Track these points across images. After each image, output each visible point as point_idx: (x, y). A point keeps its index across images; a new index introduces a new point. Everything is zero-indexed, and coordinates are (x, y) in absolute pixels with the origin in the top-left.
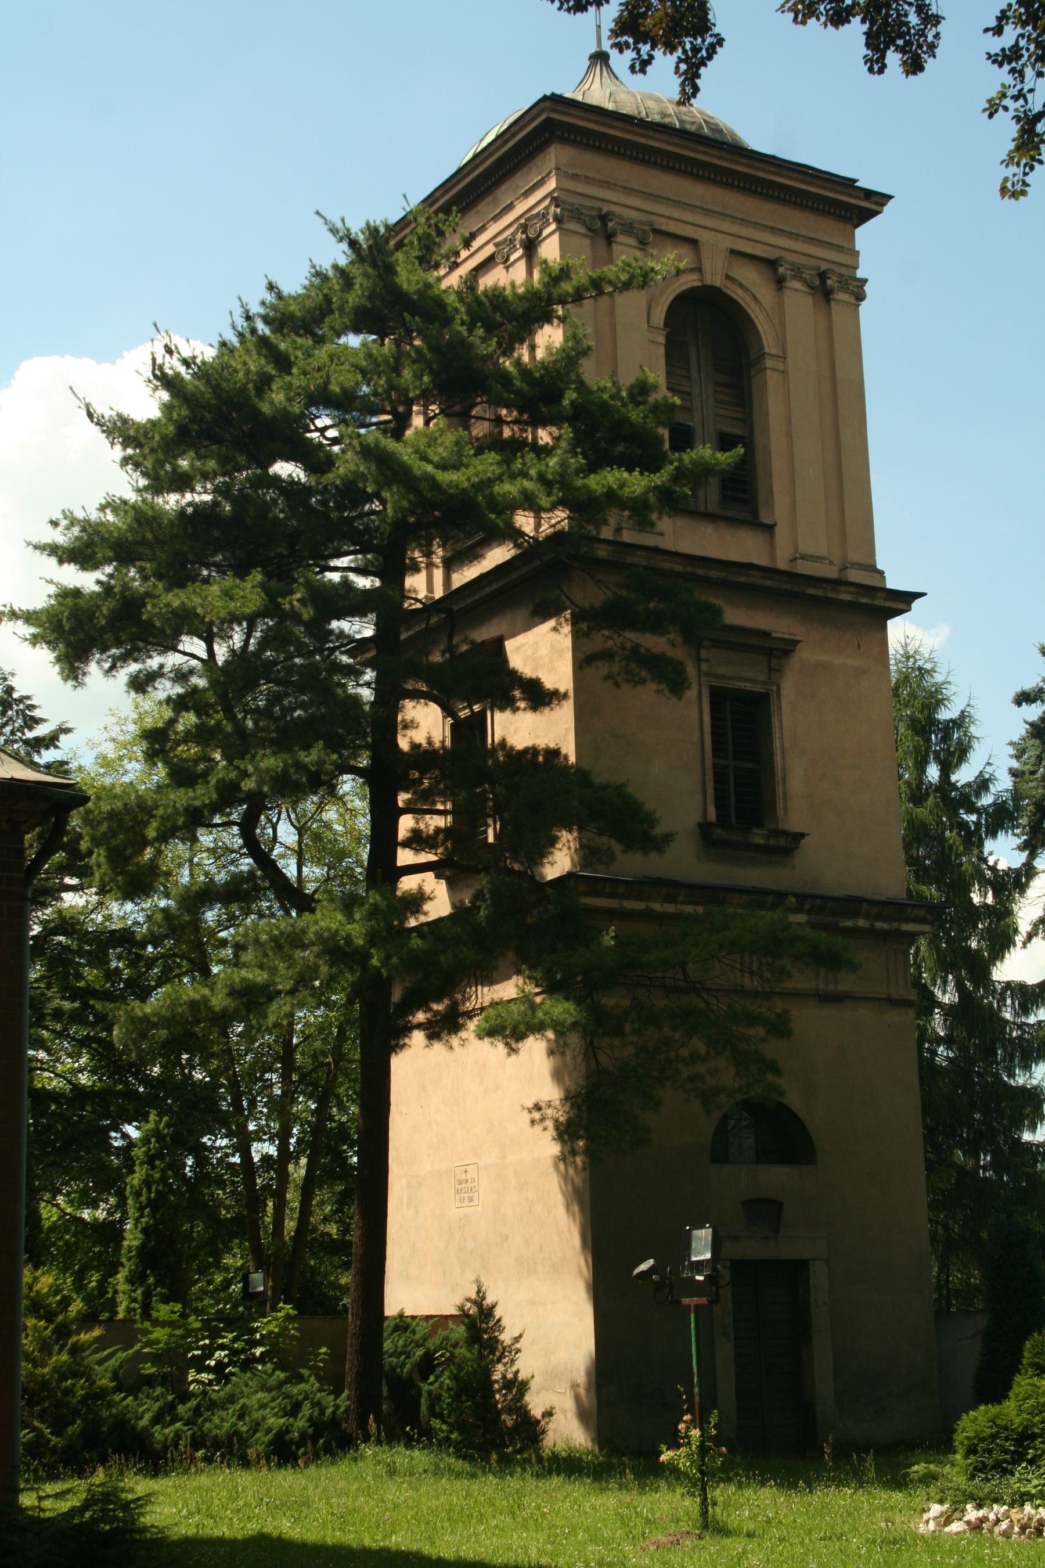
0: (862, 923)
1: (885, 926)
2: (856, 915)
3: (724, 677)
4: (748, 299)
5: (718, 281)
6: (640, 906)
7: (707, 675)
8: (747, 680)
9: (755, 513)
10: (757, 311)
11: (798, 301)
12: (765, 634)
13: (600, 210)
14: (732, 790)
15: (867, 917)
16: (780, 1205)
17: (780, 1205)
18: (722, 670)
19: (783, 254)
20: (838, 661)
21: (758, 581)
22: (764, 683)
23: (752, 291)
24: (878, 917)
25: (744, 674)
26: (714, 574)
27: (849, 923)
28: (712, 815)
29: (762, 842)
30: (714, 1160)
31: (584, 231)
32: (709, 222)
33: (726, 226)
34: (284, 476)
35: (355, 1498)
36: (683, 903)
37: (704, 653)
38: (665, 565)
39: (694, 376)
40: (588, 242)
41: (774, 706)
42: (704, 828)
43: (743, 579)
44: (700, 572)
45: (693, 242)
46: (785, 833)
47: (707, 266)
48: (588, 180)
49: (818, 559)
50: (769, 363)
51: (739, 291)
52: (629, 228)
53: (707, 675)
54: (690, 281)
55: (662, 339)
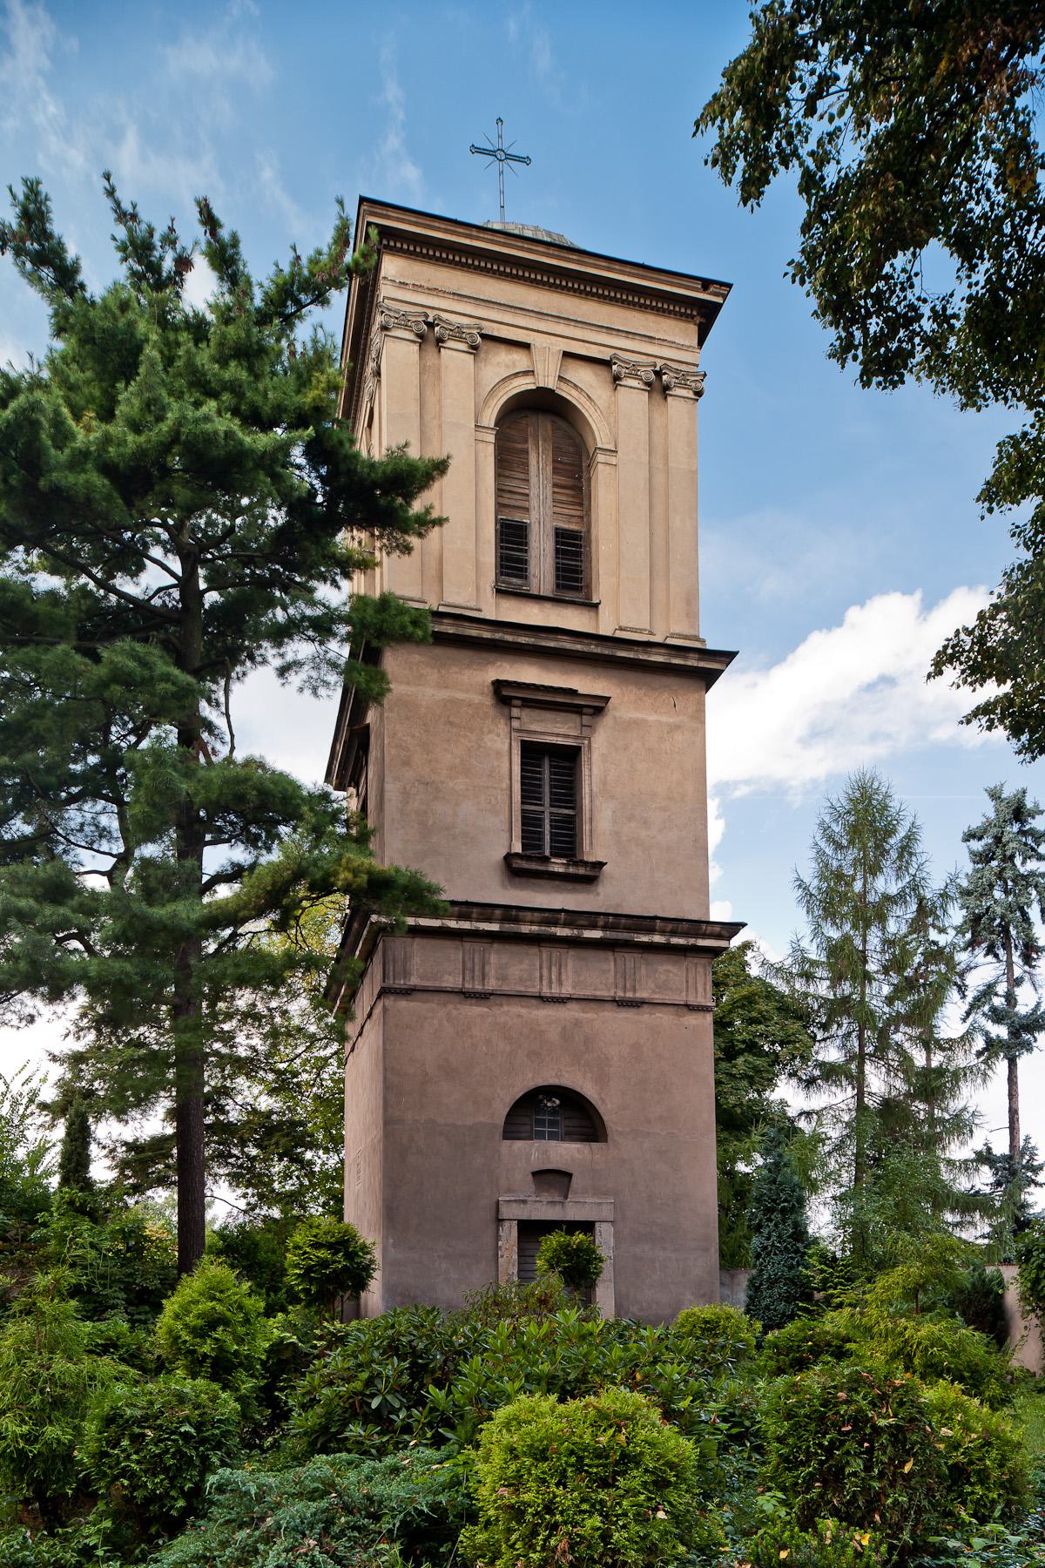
0: (657, 939)
1: (681, 941)
2: (651, 931)
3: (535, 732)
4: (583, 400)
5: (551, 383)
6: (436, 923)
7: (518, 731)
8: (558, 735)
9: (589, 596)
10: (592, 410)
11: (633, 398)
12: (573, 692)
13: (427, 316)
14: (547, 838)
15: (662, 932)
16: (570, 1175)
17: (570, 1175)
18: (533, 727)
19: (620, 353)
20: (652, 718)
21: (568, 646)
22: (576, 737)
23: (587, 391)
24: (674, 933)
25: (555, 729)
26: (523, 640)
27: (645, 939)
28: (517, 848)
29: (561, 870)
30: (505, 1138)
31: (412, 337)
32: (542, 326)
33: (561, 329)
34: (241, 847)
35: (91, 1082)
36: (478, 920)
37: (515, 712)
38: (474, 633)
39: (533, 480)
40: (416, 347)
41: (584, 758)
42: (509, 857)
43: (552, 644)
44: (509, 638)
45: (526, 346)
46: (585, 864)
47: (539, 369)
48: (417, 288)
49: (640, 631)
50: (601, 458)
51: (574, 392)
52: (458, 333)
53: (518, 731)
54: (525, 384)
55: (492, 438)
